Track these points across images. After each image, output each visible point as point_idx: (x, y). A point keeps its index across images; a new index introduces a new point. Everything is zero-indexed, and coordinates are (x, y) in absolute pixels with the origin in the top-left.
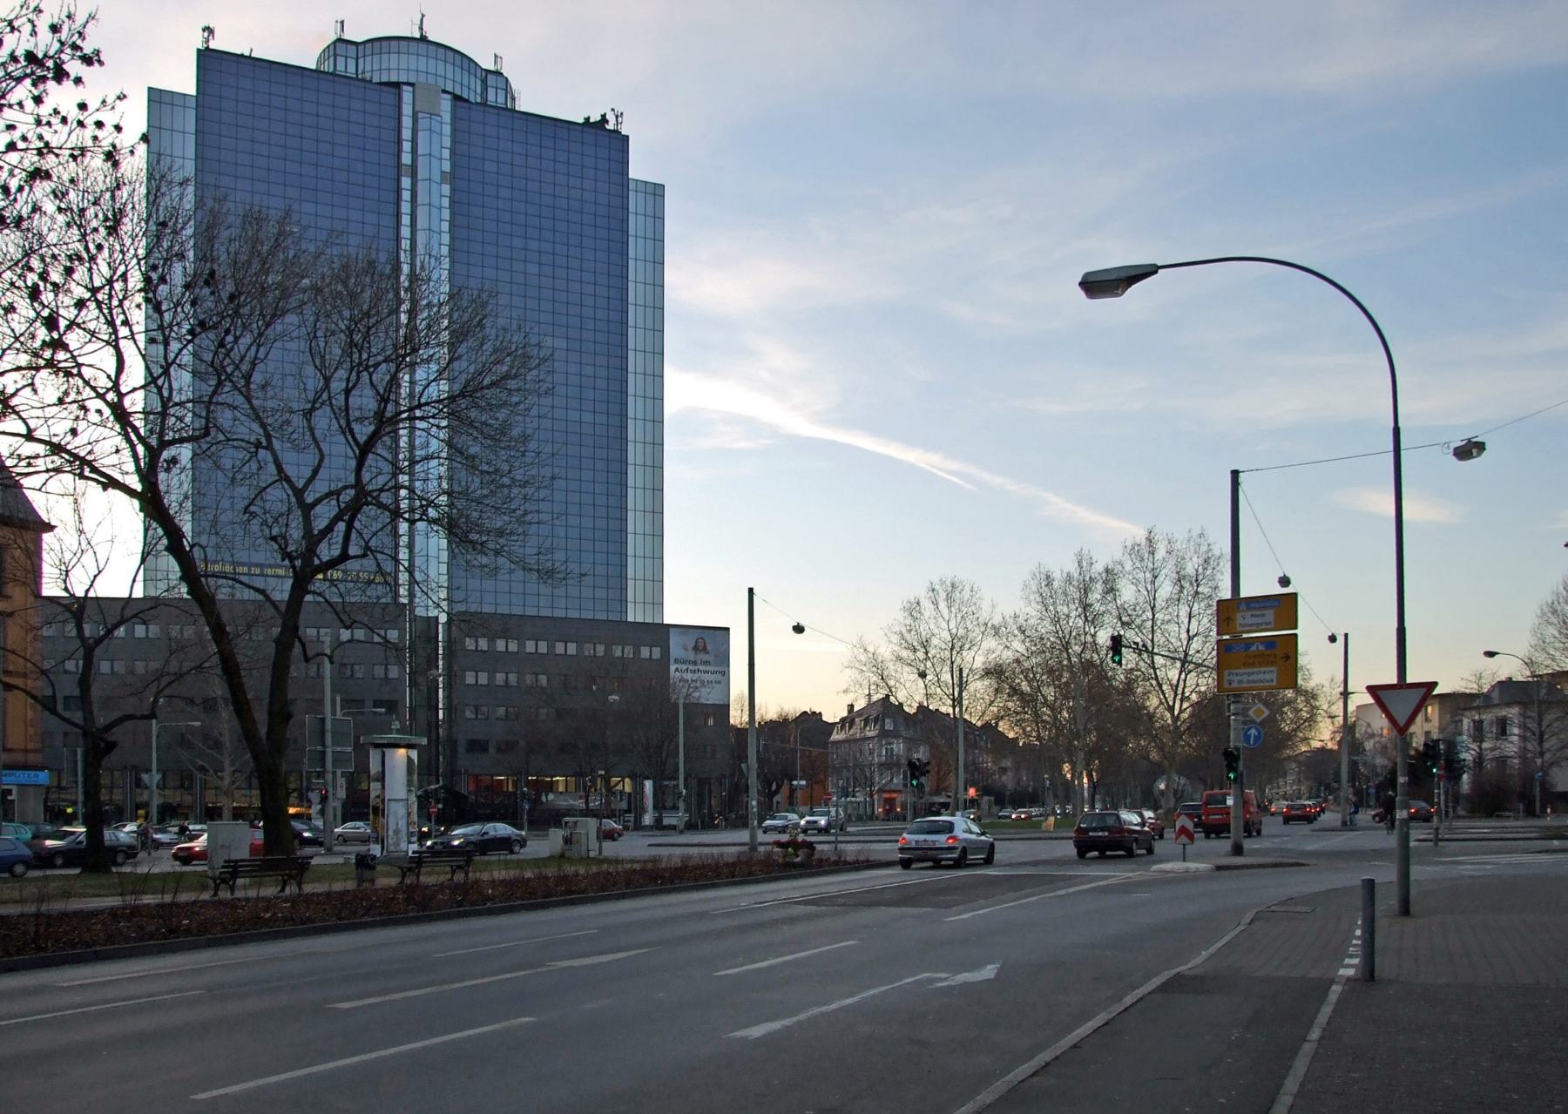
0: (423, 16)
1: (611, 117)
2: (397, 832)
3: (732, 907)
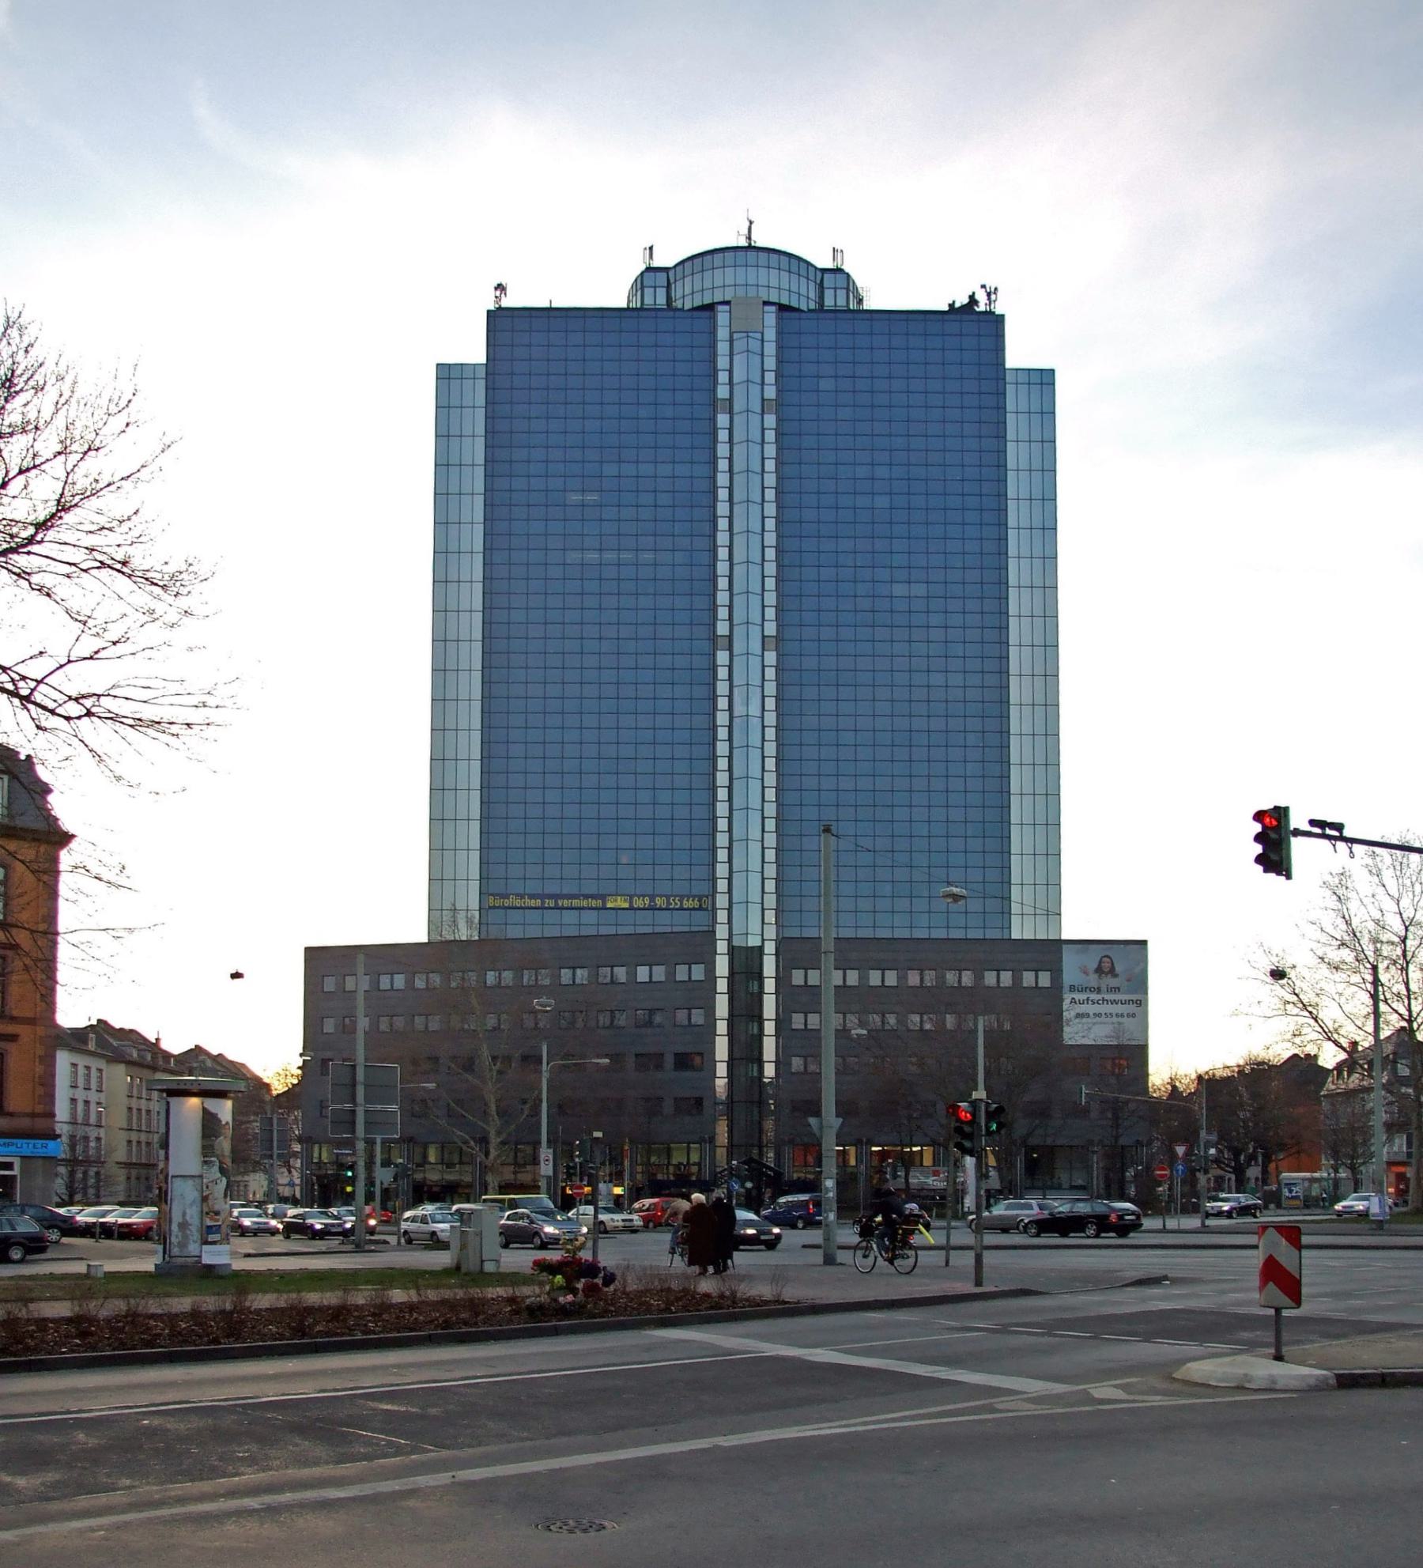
0: (751, 223)
1: (981, 297)
2: (183, 1226)
3: (201, 1401)
